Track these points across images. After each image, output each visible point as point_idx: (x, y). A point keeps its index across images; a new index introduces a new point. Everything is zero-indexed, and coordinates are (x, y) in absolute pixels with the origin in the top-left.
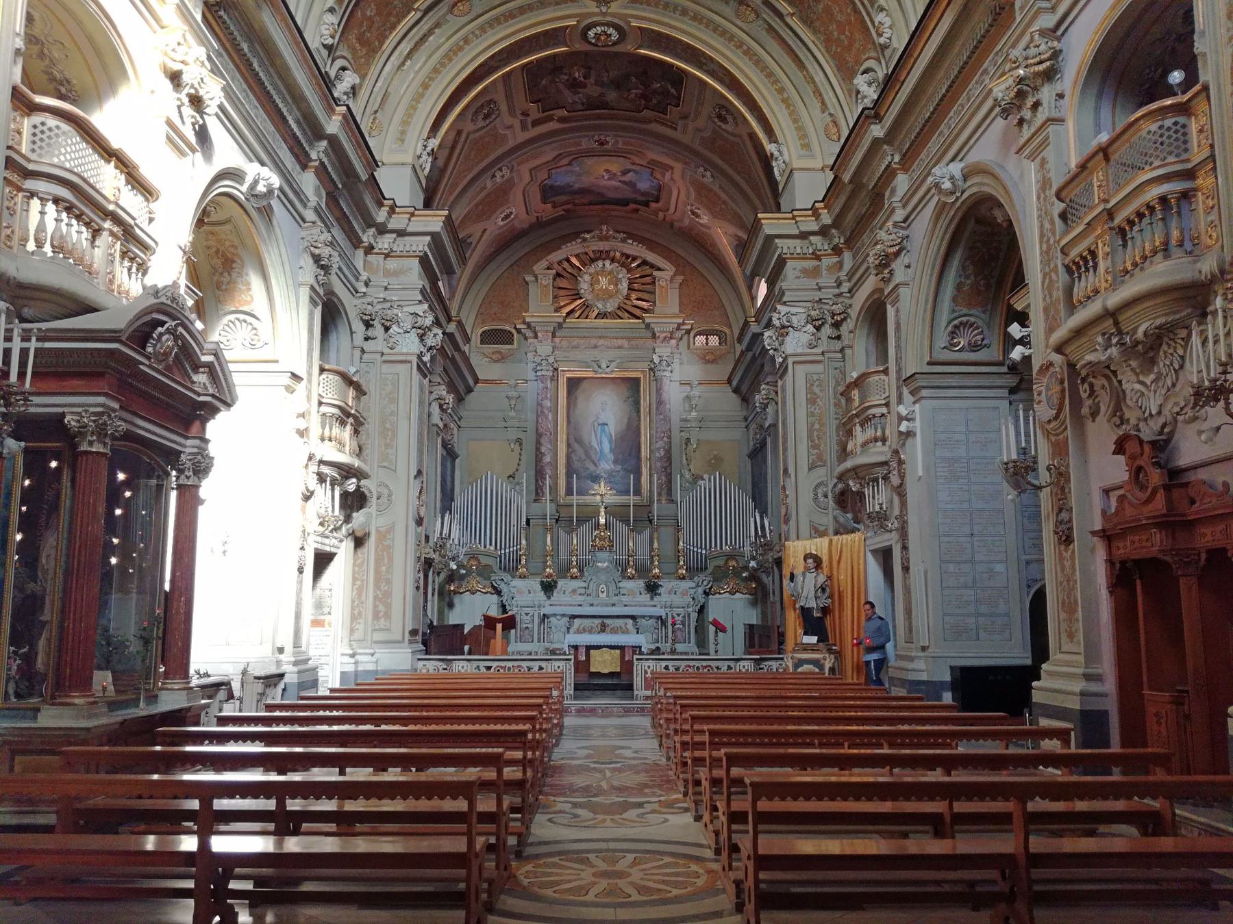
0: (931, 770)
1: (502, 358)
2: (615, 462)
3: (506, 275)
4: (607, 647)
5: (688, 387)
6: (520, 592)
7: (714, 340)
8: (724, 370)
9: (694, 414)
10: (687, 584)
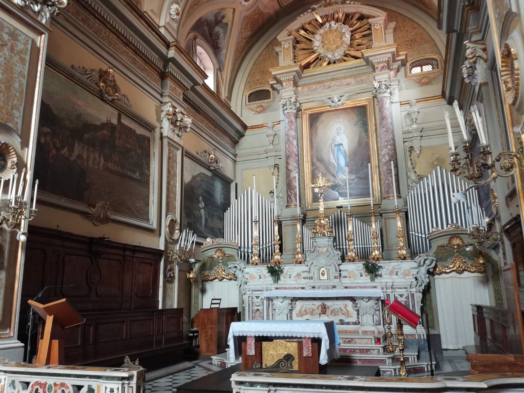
0: (497, 264)
1: (263, 110)
2: (350, 172)
3: (263, 53)
4: (284, 338)
5: (408, 106)
6: (252, 277)
7: (427, 68)
8: (436, 89)
9: (415, 126)
10: (408, 265)
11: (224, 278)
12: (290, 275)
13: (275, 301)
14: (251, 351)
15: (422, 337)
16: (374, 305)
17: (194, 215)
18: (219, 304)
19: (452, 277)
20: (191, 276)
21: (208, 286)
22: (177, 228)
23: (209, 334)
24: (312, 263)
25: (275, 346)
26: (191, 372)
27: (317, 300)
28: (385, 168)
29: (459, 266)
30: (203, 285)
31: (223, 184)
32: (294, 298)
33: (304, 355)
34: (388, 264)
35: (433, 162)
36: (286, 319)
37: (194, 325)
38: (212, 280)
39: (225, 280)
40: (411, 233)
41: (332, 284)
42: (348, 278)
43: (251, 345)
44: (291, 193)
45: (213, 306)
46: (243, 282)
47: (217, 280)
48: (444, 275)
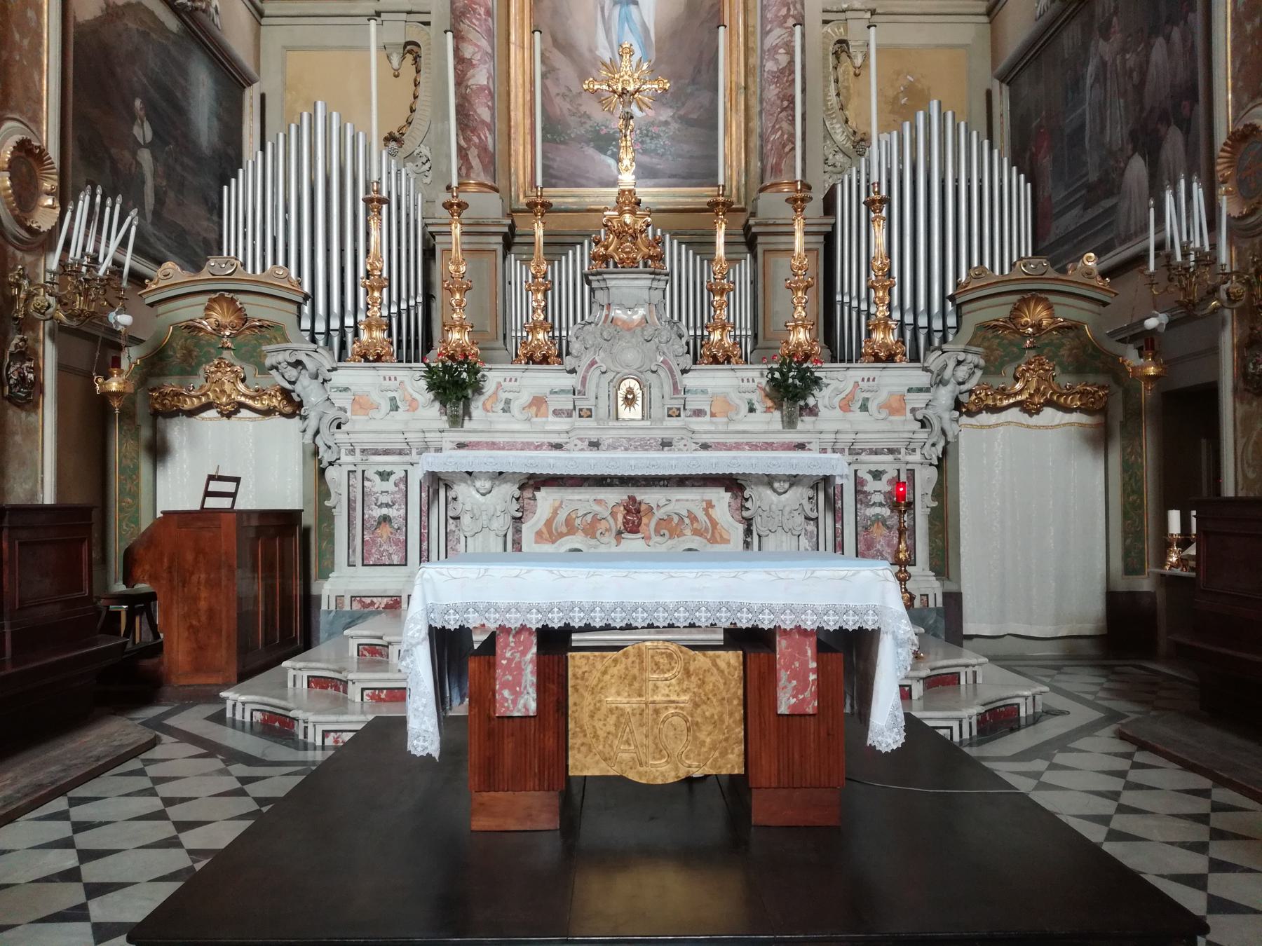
6: (362, 405)
10: (901, 377)
11: (242, 405)
12: (508, 402)
13: (463, 491)
14: (519, 699)
15: (931, 604)
16: (805, 502)
17: (114, 162)
18: (233, 495)
19: (1009, 423)
20: (114, 385)
21: (177, 432)
22: (47, 185)
23: (203, 605)
24: (593, 363)
25: (635, 671)
26: (152, 771)
27: (564, 485)
28: (772, 92)
29: (1037, 390)
30: (154, 428)
31: (216, 82)
32: (532, 476)
33: (783, 709)
34: (840, 375)
35: (896, 98)
36: (500, 548)
37: (138, 572)
38: (192, 413)
39: (244, 413)
40: (839, 298)
41: (659, 435)
42: (708, 418)
43: (520, 669)
44: (468, 140)
45: (212, 503)
46: (327, 420)
47: (212, 413)
48: (985, 418)
